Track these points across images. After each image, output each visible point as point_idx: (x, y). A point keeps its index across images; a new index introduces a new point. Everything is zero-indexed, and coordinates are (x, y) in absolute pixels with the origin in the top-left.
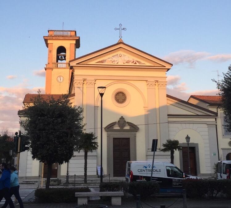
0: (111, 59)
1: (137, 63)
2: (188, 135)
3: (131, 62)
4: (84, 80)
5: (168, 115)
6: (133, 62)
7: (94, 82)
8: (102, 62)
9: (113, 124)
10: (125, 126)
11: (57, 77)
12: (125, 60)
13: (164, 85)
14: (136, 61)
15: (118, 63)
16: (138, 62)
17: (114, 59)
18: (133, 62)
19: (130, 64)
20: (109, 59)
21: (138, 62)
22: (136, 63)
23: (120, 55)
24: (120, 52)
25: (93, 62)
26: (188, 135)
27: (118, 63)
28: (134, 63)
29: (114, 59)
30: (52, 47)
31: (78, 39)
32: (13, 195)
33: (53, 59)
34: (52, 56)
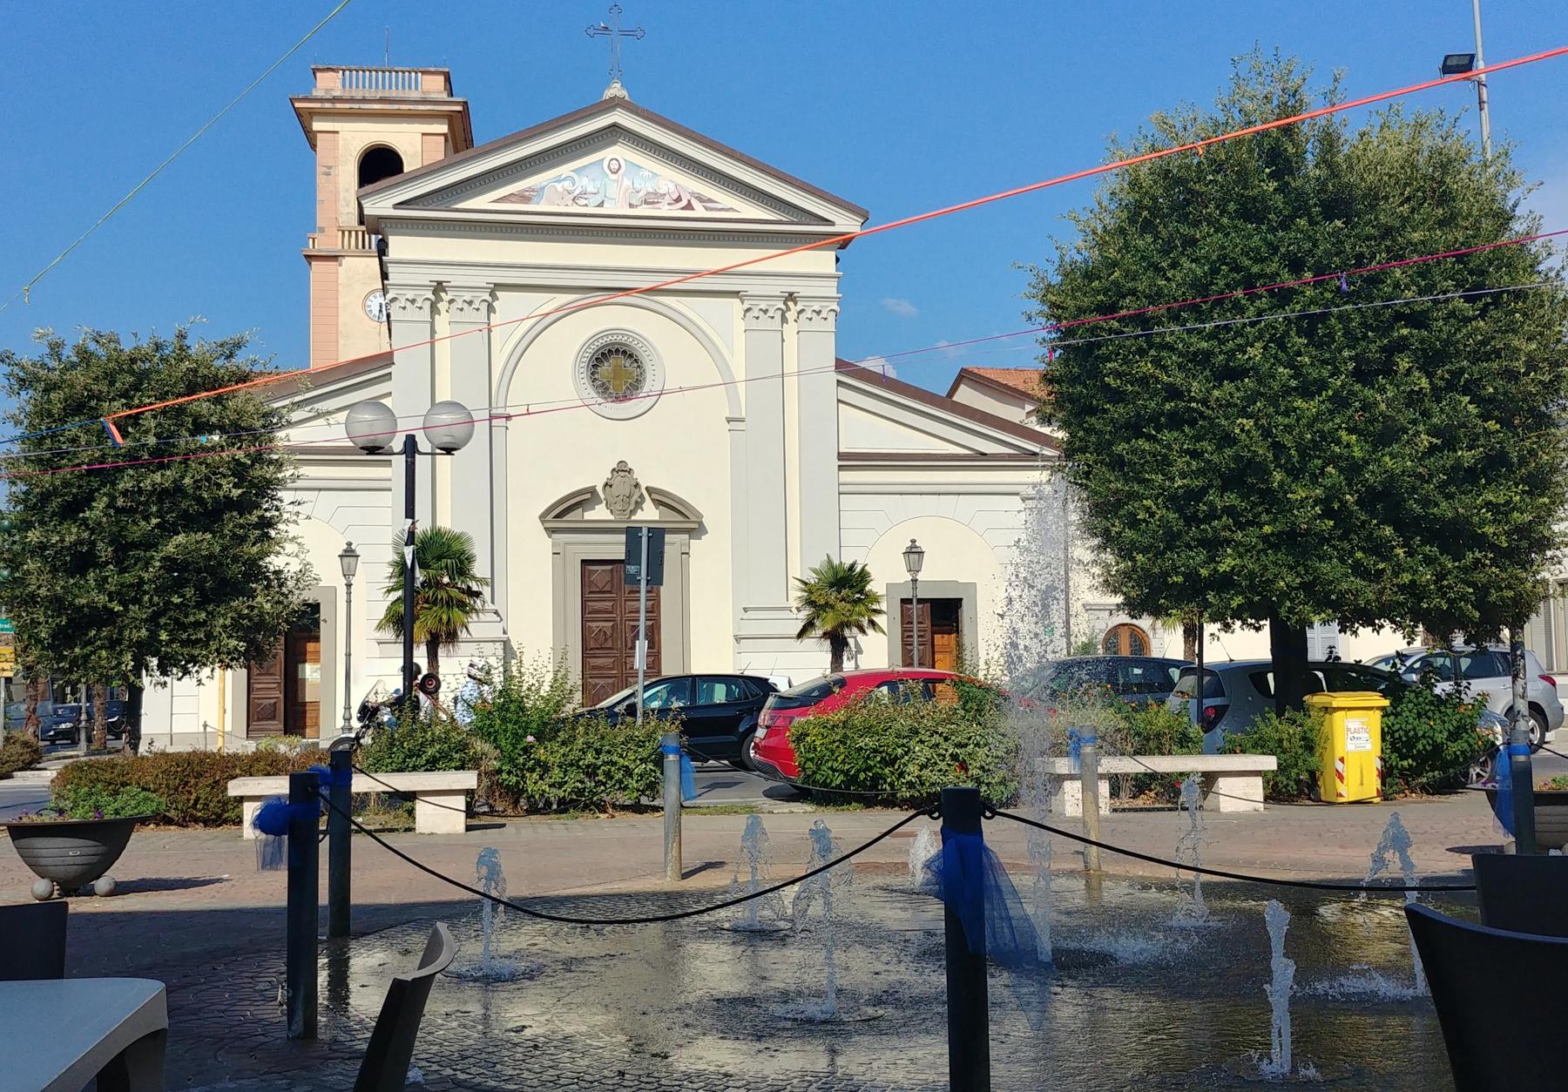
0: (567, 184)
1: (695, 203)
2: (913, 541)
3: (668, 199)
4: (439, 287)
5: (841, 456)
6: (679, 200)
7: (487, 296)
8: (523, 197)
9: (583, 499)
10: (639, 504)
11: (366, 297)
12: (637, 186)
13: (824, 315)
14: (692, 194)
15: (601, 205)
16: (700, 199)
17: (585, 183)
18: (679, 200)
19: (665, 210)
20: (559, 186)
21: (700, 199)
22: (689, 207)
23: (614, 166)
24: (617, 151)
25: (482, 202)
26: (913, 541)
27: (601, 205)
28: (684, 203)
29: (585, 183)
30: (336, 148)
31: (459, 108)
32: (1512, 851)
33: (344, 210)
34: (336, 193)
